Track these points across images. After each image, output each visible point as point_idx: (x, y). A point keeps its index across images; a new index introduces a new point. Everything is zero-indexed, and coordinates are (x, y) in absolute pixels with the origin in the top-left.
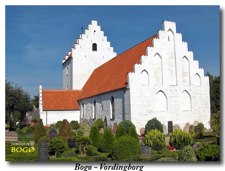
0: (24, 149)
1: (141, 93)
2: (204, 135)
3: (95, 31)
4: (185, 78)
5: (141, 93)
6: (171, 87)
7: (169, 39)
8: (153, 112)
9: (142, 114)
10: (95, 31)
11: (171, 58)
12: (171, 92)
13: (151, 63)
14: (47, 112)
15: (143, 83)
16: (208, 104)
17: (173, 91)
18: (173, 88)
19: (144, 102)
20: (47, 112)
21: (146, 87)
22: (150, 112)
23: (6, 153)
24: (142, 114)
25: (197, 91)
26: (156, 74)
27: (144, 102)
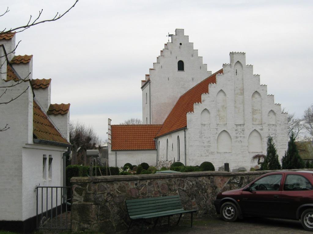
0: (89, 190)
1: (201, 133)
2: (191, 213)
3: (181, 44)
4: (255, 116)
5: (201, 133)
6: (237, 126)
7: (236, 72)
8: (214, 153)
9: (201, 156)
10: (181, 44)
11: (239, 94)
12: (237, 132)
13: (213, 101)
14: (116, 153)
15: (203, 123)
16: (285, 145)
17: (239, 130)
18: (239, 127)
19: (204, 143)
20: (116, 153)
21: (207, 127)
22: (211, 153)
23: (207, 68)
24: (201, 156)
25: (270, 130)
26: (219, 113)
27: (204, 143)
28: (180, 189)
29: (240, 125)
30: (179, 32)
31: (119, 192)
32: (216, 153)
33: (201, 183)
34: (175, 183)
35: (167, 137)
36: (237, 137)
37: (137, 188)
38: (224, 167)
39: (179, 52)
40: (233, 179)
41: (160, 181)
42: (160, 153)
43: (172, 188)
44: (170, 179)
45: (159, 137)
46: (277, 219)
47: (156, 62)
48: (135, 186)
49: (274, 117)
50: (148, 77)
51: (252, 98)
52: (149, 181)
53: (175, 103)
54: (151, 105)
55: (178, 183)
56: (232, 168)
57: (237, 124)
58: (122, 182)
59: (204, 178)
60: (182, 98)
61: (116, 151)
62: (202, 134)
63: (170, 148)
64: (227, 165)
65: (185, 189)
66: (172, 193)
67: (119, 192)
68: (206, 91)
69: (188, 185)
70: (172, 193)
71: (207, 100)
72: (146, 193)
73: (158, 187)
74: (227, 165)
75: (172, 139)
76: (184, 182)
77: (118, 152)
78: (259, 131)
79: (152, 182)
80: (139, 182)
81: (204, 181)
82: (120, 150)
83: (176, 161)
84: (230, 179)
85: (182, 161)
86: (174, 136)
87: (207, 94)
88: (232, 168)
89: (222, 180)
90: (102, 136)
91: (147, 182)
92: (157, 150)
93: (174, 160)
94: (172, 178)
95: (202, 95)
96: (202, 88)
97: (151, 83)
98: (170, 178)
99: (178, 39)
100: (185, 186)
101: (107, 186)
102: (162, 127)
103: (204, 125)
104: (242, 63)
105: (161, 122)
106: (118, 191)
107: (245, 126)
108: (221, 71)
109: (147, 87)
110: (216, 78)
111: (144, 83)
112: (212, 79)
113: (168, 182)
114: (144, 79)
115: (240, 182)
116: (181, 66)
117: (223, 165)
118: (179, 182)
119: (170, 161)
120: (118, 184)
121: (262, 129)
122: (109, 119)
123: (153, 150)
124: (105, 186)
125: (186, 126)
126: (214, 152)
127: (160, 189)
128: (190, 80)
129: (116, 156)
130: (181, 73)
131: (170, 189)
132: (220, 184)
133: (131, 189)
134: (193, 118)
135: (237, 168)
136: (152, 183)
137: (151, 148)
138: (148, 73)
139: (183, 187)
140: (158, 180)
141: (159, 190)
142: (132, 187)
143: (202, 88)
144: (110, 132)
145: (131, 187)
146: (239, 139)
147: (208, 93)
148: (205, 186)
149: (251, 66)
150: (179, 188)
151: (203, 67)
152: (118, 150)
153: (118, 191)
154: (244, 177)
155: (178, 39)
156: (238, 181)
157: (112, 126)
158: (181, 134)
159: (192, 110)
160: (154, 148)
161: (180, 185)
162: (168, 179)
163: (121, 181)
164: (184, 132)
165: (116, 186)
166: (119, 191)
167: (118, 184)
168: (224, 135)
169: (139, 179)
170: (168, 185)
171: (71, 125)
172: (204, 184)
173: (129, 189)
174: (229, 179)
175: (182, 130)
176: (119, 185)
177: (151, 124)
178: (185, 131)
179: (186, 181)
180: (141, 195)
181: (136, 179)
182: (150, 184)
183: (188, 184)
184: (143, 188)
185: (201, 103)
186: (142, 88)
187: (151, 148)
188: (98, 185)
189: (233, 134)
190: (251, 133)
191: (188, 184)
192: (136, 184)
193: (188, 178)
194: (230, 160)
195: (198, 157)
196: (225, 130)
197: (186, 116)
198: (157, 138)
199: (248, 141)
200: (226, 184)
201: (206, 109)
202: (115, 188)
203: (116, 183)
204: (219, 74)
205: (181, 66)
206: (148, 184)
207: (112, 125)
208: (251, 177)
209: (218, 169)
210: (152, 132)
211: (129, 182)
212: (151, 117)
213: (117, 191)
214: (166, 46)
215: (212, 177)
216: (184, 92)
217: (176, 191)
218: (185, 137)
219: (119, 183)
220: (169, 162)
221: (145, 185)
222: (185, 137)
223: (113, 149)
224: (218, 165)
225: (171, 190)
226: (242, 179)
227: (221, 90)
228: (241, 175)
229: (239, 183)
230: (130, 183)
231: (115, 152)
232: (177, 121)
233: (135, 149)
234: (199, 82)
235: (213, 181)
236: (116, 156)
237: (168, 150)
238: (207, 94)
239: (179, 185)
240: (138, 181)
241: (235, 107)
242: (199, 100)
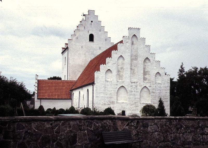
6: (132, 83)
10: (92, 22)
12: (132, 87)
13: (115, 64)
17: (134, 86)
18: (133, 84)
28: (89, 129)
29: (135, 82)
30: (91, 12)
31: (36, 130)
32: (116, 103)
33: (105, 125)
34: (84, 124)
35: (80, 90)
36: (132, 91)
37: (52, 128)
38: (121, 113)
39: (90, 27)
40: (131, 123)
41: (72, 122)
42: (74, 102)
43: (82, 128)
44: (81, 120)
45: (73, 90)
46: (110, 143)
47: (73, 34)
48: (50, 126)
49: (160, 77)
50: (67, 45)
51: (144, 62)
52: (63, 122)
53: (86, 65)
54: (68, 66)
55: (87, 124)
56: (128, 114)
57: (132, 81)
58: (38, 122)
59: (108, 120)
60: (91, 62)
61: (41, 99)
62: (106, 89)
63: (81, 98)
64: (123, 113)
65: (92, 130)
66: (81, 132)
67: (36, 130)
68: (110, 56)
69: (95, 126)
70: (81, 132)
71: (111, 62)
72: (60, 132)
73: (70, 127)
74: (123, 113)
75: (83, 91)
76: (91, 123)
77: (42, 100)
78: (148, 87)
79: (65, 122)
80: (54, 123)
81: (108, 123)
82: (43, 99)
83: (85, 107)
84: (129, 123)
85: (90, 107)
86: (85, 89)
87: (110, 58)
88: (128, 114)
89: (122, 123)
90: (31, 88)
91: (60, 122)
92: (71, 99)
93: (84, 107)
94: (82, 120)
95: (107, 59)
96: (107, 54)
97: (69, 50)
98: (80, 119)
99: (90, 17)
100: (93, 127)
101: (25, 125)
102: (76, 83)
103: (108, 81)
104: (137, 36)
105: (75, 79)
106: (35, 130)
107: (138, 83)
108: (121, 42)
109: (66, 53)
110: (118, 47)
111: (64, 49)
112: (115, 47)
113: (78, 123)
114: (64, 47)
115: (136, 125)
116: (91, 38)
117: (121, 112)
118: (88, 123)
119: (81, 107)
120: (35, 124)
121: (150, 86)
122: (36, 75)
123: (69, 99)
124: (24, 125)
125: (94, 82)
126: (114, 102)
127: (72, 128)
128: (98, 48)
129: (41, 103)
130: (91, 43)
131: (80, 128)
132: (121, 126)
133: (46, 128)
134: (99, 76)
135: (132, 115)
136: (65, 123)
137: (65, 98)
138: (67, 42)
139: (91, 128)
140: (70, 121)
141: (70, 129)
142: (48, 126)
143: (107, 54)
144: (37, 85)
145: (47, 127)
146: (133, 93)
147: (111, 58)
148: (108, 127)
149: (144, 39)
150: (87, 129)
151: (107, 39)
152: (42, 99)
153: (35, 130)
154: (140, 121)
155: (90, 17)
156: (135, 125)
157: (38, 80)
158: (90, 88)
159: (98, 70)
160: (70, 98)
161: (88, 126)
162: (79, 121)
163: (38, 121)
164: (92, 86)
165: (34, 125)
166: (36, 130)
167: (35, 124)
168: (122, 90)
169: (54, 120)
170: (78, 125)
171: (55, 61)
172: (108, 125)
173: (45, 128)
174: (128, 122)
175: (91, 84)
176: (36, 125)
177: (68, 80)
178: (93, 86)
179: (93, 122)
180: (55, 133)
181: (51, 120)
182: (63, 124)
183: (95, 125)
184: (57, 127)
185: (106, 65)
186: (62, 53)
187: (65, 98)
188: (17, 124)
189: (129, 89)
190: (142, 89)
191: (95, 125)
192: (51, 124)
193: (95, 120)
194: (126, 108)
195: (102, 105)
196: (123, 86)
197: (94, 75)
198: (72, 90)
199: (140, 94)
200: (125, 126)
201: (109, 69)
202: (33, 127)
203: (33, 123)
204: (120, 43)
205: (91, 38)
206: (62, 125)
207: (38, 80)
208: (145, 122)
209: (117, 114)
210: (50, 89)
211: (45, 122)
212: (68, 75)
213: (34, 130)
214: (81, 23)
215: (114, 120)
216: (93, 57)
217: (85, 130)
218: (93, 90)
219: (36, 123)
220: (81, 108)
221: (59, 125)
222: (93, 90)
223: (39, 98)
224: (117, 111)
225: (81, 130)
226: (138, 122)
227: (121, 56)
228: (137, 119)
229: (136, 126)
230: (46, 123)
231: (40, 100)
232: (87, 79)
233: (59, 98)
234: (105, 50)
235: (115, 123)
236: (41, 103)
237: (80, 99)
238: (110, 58)
239: (87, 126)
240: (53, 122)
241: (131, 69)
242: (104, 63)
